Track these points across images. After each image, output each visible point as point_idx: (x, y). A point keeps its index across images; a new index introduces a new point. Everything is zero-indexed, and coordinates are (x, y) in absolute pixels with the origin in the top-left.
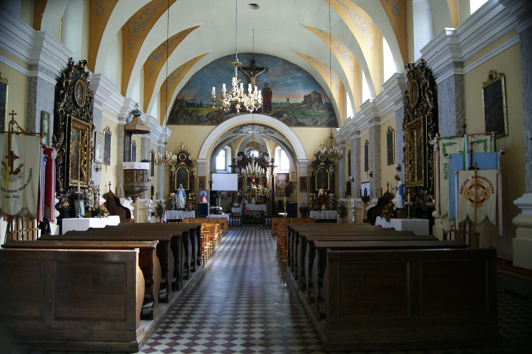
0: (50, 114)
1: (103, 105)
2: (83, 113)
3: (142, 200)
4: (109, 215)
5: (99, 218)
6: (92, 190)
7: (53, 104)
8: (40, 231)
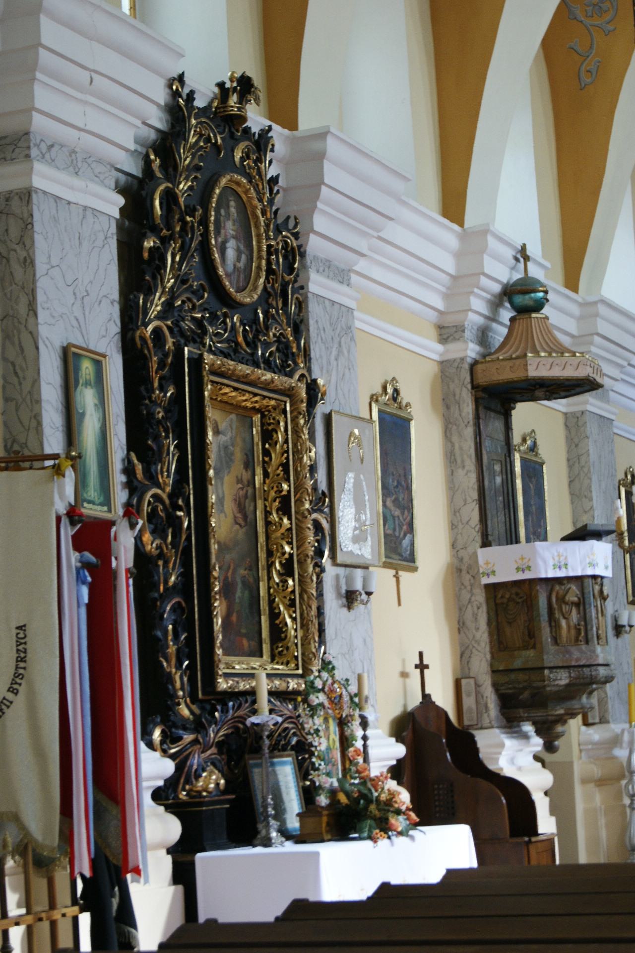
0: (104, 356)
1: (354, 278)
2: (258, 332)
3: (595, 734)
4: (415, 825)
5: (369, 843)
6: (327, 704)
7: (116, 310)
8: (85, 920)
